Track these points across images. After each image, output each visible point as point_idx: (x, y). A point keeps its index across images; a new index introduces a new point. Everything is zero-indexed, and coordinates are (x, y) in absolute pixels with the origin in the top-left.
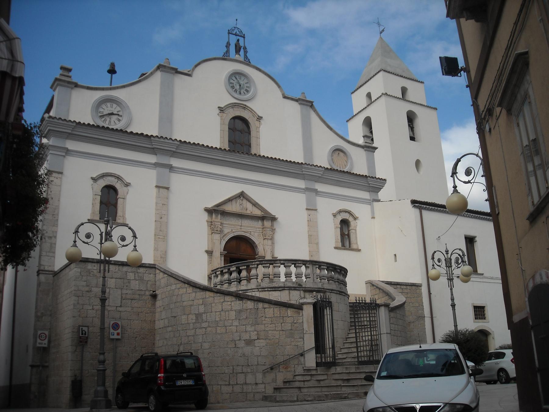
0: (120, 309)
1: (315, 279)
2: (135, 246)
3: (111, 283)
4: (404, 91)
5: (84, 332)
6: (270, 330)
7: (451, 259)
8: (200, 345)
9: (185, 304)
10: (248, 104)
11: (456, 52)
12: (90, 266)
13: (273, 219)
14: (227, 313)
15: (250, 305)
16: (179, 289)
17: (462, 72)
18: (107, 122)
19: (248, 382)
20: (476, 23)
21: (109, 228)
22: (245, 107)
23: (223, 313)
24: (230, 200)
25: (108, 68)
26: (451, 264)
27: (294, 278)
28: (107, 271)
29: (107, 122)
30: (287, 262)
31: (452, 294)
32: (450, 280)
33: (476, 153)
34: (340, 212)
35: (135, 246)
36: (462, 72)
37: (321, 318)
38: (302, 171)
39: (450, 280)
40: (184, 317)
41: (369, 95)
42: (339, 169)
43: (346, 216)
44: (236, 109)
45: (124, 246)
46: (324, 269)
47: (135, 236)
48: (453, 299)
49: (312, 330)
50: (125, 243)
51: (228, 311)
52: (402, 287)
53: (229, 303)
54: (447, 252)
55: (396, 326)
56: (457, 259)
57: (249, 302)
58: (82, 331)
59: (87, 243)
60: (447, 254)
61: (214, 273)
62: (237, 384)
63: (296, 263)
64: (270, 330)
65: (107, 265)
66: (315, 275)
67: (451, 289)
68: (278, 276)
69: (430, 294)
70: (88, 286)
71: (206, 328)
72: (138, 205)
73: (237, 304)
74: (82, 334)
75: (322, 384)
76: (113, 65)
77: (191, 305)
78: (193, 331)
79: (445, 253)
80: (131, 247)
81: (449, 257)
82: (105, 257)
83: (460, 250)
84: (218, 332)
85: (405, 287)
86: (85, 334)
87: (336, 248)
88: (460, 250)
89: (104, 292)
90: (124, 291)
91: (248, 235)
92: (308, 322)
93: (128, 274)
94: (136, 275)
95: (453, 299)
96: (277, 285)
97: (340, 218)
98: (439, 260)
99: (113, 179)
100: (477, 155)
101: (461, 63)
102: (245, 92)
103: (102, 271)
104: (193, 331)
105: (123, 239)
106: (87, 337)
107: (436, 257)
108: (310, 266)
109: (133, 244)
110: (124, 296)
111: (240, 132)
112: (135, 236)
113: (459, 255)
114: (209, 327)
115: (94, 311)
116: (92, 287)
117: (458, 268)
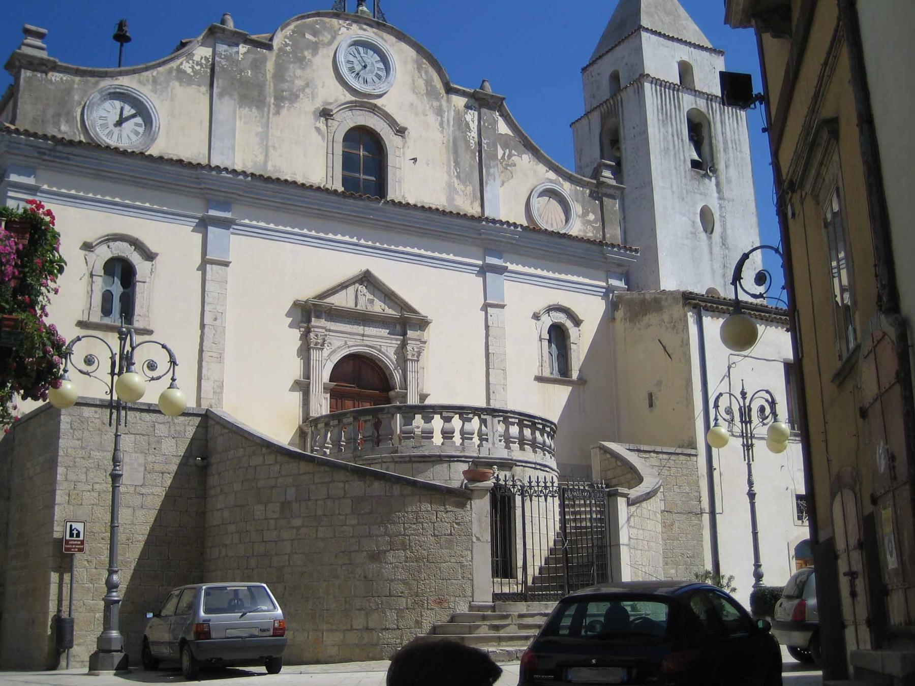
0: (143, 491)
1: (497, 441)
2: (173, 379)
3: (126, 442)
4: (685, 70)
5: (75, 532)
6: (412, 534)
7: (750, 410)
8: (287, 557)
9: (261, 484)
10: (378, 102)
11: (750, 66)
12: (87, 412)
13: (423, 324)
14: (337, 501)
15: (377, 487)
16: (249, 456)
17: (757, 103)
18: (115, 137)
19: (371, 626)
20: (775, 40)
21: (128, 348)
22: (374, 109)
23: (329, 502)
24: (343, 286)
25: (115, 30)
26: (750, 417)
27: (457, 439)
28: (123, 422)
29: (115, 137)
30: (447, 411)
31: (750, 475)
32: (748, 447)
33: (775, 245)
34: (551, 309)
35: (173, 379)
36: (757, 103)
37: (496, 524)
38: (480, 234)
39: (748, 447)
40: (259, 508)
41: (615, 78)
42: (550, 229)
43: (560, 318)
44: (358, 112)
45: (153, 379)
46: (513, 424)
47: (173, 362)
48: (750, 483)
49: (488, 537)
50: (155, 374)
51: (339, 499)
52: (661, 456)
53: (341, 485)
54: (743, 394)
55: (641, 531)
56: (762, 409)
57: (376, 484)
58: (71, 530)
59: (87, 374)
60: (744, 398)
61: (309, 426)
62: (352, 629)
63: (464, 412)
64: (412, 534)
65: (123, 413)
66: (497, 435)
67: (749, 465)
68: (428, 435)
69: (710, 469)
70: (84, 448)
71: (298, 529)
72: (166, 296)
73: (357, 487)
74: (71, 535)
75: (502, 633)
76: (121, 25)
77: (273, 487)
78: (275, 533)
79: (739, 397)
80: (167, 380)
81: (747, 404)
82: (586, 632)
83: (767, 392)
84: (321, 535)
85: (665, 456)
86: (78, 535)
87: (540, 379)
88: (767, 392)
89: (116, 461)
90: (151, 458)
91: (374, 352)
92: (480, 521)
93: (157, 426)
94: (172, 429)
95: (750, 483)
96: (427, 453)
97: (547, 321)
98: (729, 411)
99: (126, 245)
100: (777, 251)
101: (757, 88)
102: (375, 79)
103: (114, 422)
104: (275, 533)
105: (152, 366)
106: (82, 542)
107: (724, 403)
108: (488, 418)
109: (170, 374)
110: (149, 467)
111: (366, 157)
112: (173, 362)
113: (767, 401)
114: (303, 526)
115: (95, 495)
116: (91, 449)
117: (764, 424)
